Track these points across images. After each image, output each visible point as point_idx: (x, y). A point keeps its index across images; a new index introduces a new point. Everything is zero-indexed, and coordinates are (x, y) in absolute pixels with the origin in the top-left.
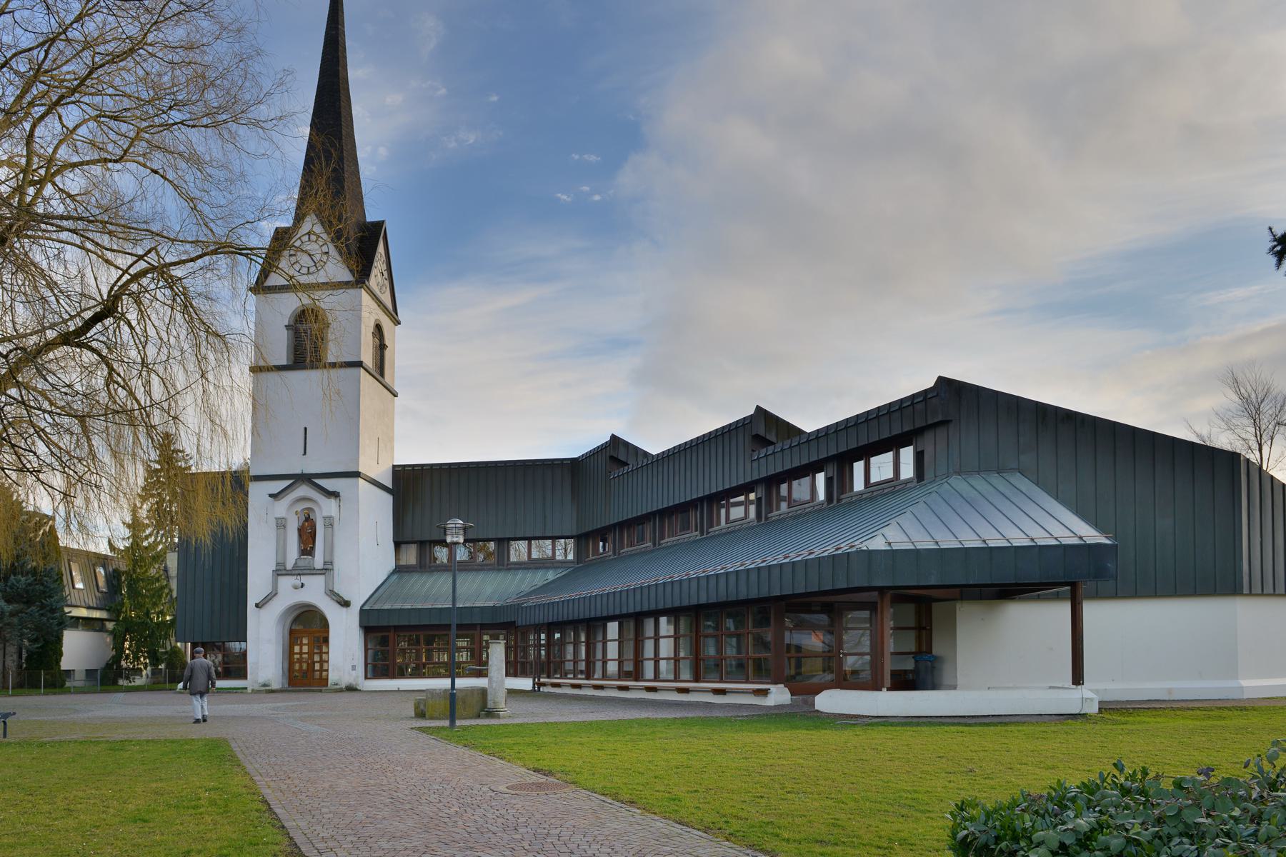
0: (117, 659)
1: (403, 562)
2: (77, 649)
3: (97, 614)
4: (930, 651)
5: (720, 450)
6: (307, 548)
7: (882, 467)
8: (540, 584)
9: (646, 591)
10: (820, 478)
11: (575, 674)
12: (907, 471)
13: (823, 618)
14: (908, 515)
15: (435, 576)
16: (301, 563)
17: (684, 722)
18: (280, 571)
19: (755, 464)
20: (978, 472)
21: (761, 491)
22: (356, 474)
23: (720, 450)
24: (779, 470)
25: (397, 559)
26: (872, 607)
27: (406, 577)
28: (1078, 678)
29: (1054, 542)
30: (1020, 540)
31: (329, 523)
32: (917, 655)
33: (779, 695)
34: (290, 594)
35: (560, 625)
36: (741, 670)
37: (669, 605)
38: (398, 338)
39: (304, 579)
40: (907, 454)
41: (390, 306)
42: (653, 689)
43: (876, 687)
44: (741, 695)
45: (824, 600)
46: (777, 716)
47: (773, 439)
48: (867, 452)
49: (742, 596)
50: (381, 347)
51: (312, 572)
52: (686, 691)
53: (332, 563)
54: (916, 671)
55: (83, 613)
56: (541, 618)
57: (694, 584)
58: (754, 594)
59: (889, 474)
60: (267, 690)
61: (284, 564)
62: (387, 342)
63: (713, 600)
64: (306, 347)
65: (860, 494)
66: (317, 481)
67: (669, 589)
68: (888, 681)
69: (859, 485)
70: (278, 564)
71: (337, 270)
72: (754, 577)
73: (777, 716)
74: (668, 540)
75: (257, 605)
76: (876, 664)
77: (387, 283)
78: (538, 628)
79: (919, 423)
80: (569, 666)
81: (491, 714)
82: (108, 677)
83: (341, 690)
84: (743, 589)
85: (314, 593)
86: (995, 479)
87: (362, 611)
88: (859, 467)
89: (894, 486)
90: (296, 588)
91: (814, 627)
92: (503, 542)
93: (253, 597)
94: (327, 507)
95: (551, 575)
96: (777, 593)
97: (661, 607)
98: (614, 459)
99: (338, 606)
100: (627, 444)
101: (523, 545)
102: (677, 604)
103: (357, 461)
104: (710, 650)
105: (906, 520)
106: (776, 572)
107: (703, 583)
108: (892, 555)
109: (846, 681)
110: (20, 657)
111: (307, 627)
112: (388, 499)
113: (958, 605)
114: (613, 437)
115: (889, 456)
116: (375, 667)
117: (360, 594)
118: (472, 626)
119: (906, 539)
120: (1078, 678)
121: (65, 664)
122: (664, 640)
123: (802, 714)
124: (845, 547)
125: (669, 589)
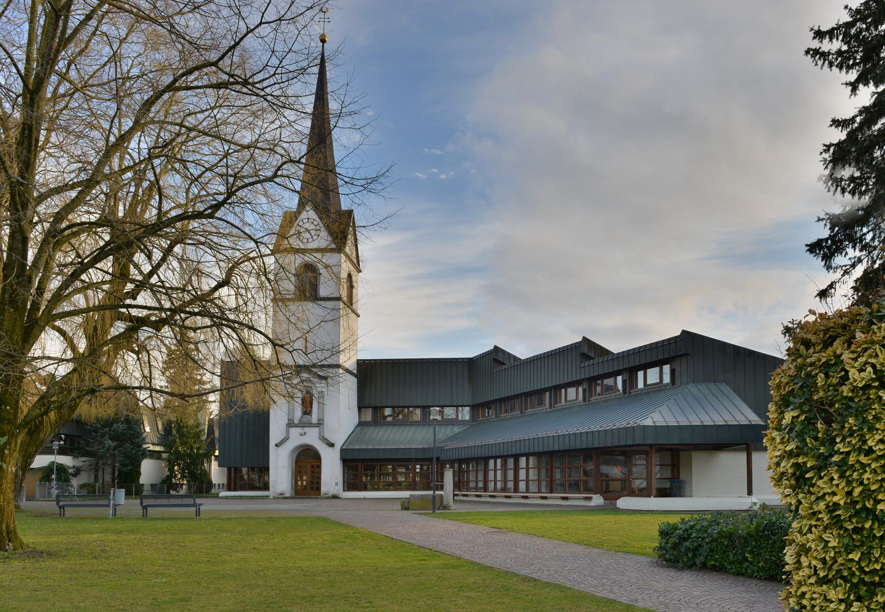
0: (169, 478)
1: (363, 420)
2: (149, 471)
3: (158, 448)
4: (678, 478)
5: (562, 360)
6: (307, 411)
7: (653, 375)
8: (450, 435)
9: (522, 442)
10: (619, 379)
11: (476, 489)
12: (667, 379)
13: (622, 458)
14: (665, 406)
15: (384, 428)
17: (551, 512)
18: (291, 424)
19: (582, 370)
20: (704, 382)
21: (586, 385)
22: (338, 366)
23: (562, 360)
24: (596, 374)
25: (360, 417)
26: (646, 453)
27: (366, 429)
28: (750, 492)
29: (736, 423)
30: (719, 422)
31: (321, 395)
32: (671, 480)
33: (597, 500)
34: (297, 438)
35: (467, 461)
36: (575, 487)
37: (536, 450)
38: (360, 280)
39: (306, 430)
40: (667, 368)
42: (526, 497)
43: (649, 496)
44: (577, 500)
45: (623, 450)
46: (597, 509)
47: (593, 355)
48: (645, 367)
49: (578, 447)
50: (351, 287)
51: (310, 425)
52: (545, 498)
54: (671, 488)
55: (152, 448)
56: (456, 456)
57: (551, 439)
58: (584, 446)
60: (282, 497)
61: (293, 420)
62: (354, 284)
63: (562, 448)
64: (308, 286)
65: (642, 390)
67: (536, 442)
68: (654, 492)
69: (641, 385)
70: (289, 420)
71: (323, 240)
72: (584, 436)
73: (597, 509)
74: (530, 411)
75: (276, 445)
76: (649, 484)
78: (417, 461)
79: (672, 355)
80: (472, 485)
81: (445, 508)
82: (165, 487)
83: (329, 498)
84: (572, 441)
85: (311, 438)
86: (712, 386)
87: (342, 450)
88: (641, 374)
89: (659, 387)
90: (301, 435)
91: (616, 464)
92: (425, 408)
93: (273, 441)
94: (319, 387)
96: (597, 446)
97: (532, 451)
98: (496, 361)
100: (503, 351)
102: (541, 450)
104: (558, 476)
105: (664, 409)
106: (596, 435)
107: (556, 439)
108: (656, 428)
109: (633, 493)
110: (114, 474)
111: (307, 461)
112: (354, 380)
113: (693, 453)
114: (495, 347)
115: (657, 369)
116: (348, 484)
117: (340, 438)
118: (409, 460)
119: (662, 419)
120: (750, 492)
121: (142, 480)
122: (528, 470)
123: (611, 508)
124: (632, 424)
125: (536, 442)
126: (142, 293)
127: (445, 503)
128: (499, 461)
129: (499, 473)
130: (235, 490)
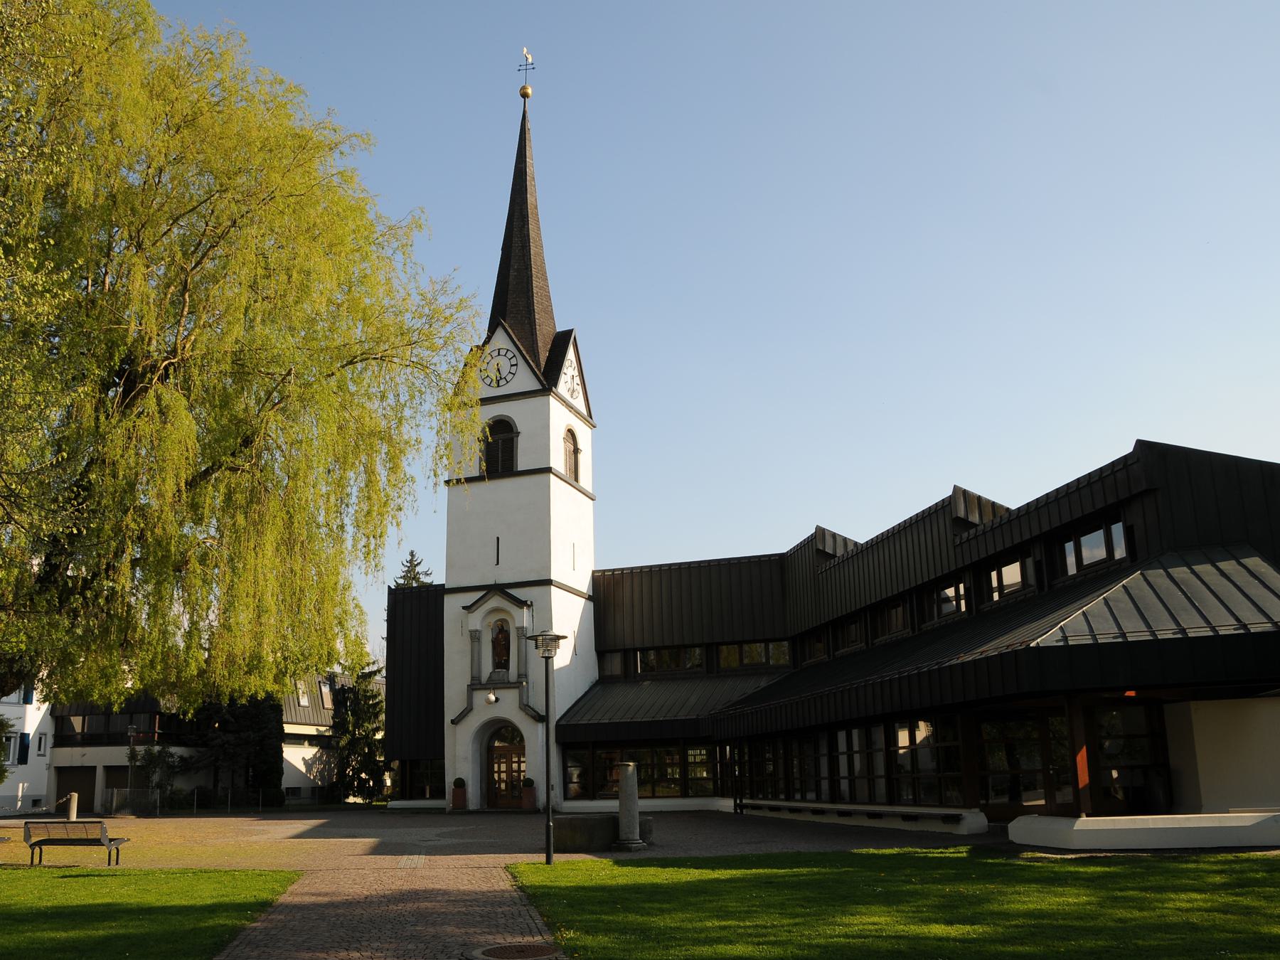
1: (608, 673)
6: (501, 660)
7: (1093, 549)
16: (495, 677)
18: (476, 685)
41: (584, 411)
51: (508, 685)
53: (526, 676)
59: (1101, 553)
61: (479, 678)
66: (481, 594)
70: (473, 678)
75: (453, 722)
77: (579, 388)
93: (450, 713)
95: (763, 683)
99: (532, 721)
101: (760, 647)
103: (548, 568)
115: (1100, 534)
126: (1018, 579)
127: (623, 836)
128: (855, 733)
129: (857, 758)
130: (411, 798)
